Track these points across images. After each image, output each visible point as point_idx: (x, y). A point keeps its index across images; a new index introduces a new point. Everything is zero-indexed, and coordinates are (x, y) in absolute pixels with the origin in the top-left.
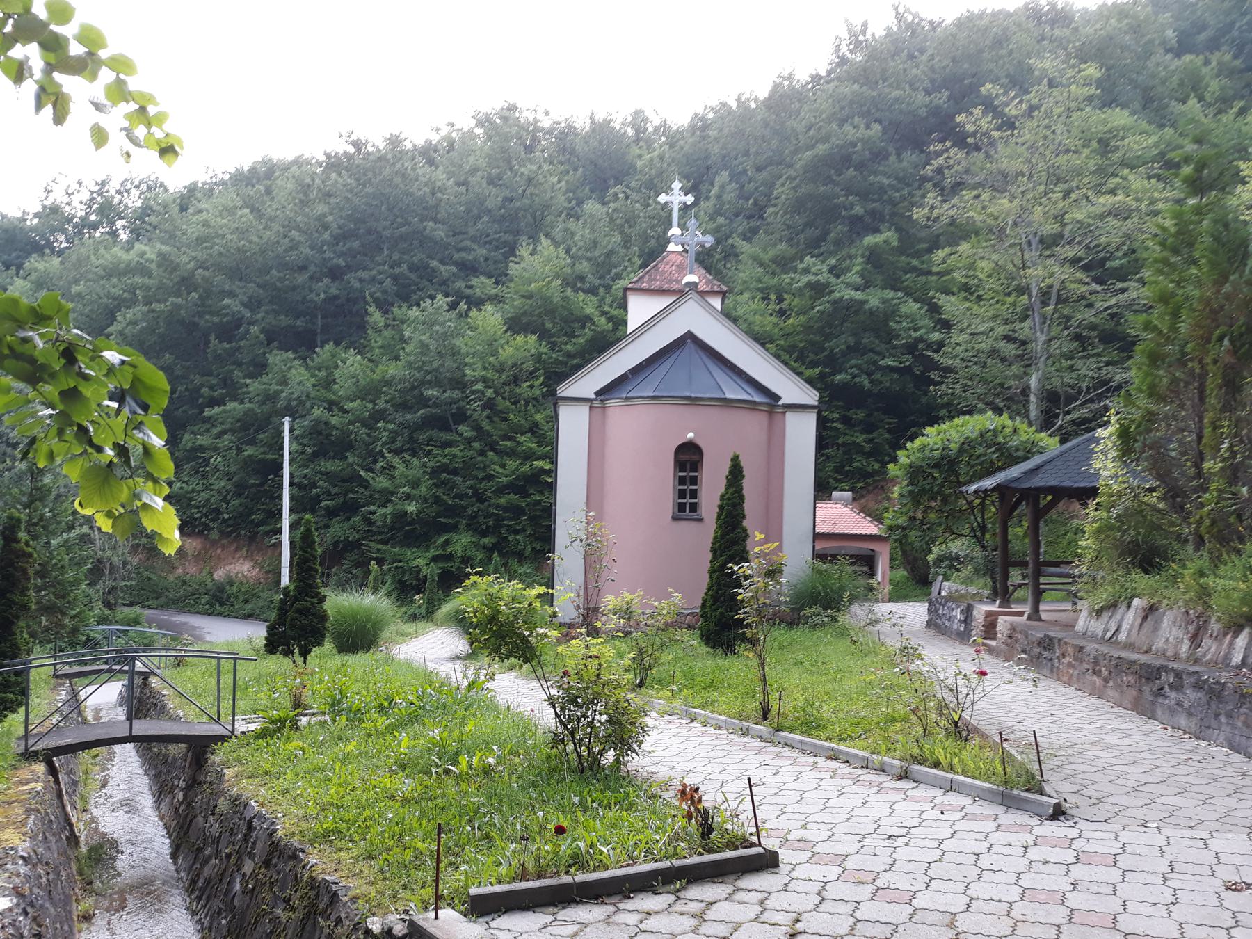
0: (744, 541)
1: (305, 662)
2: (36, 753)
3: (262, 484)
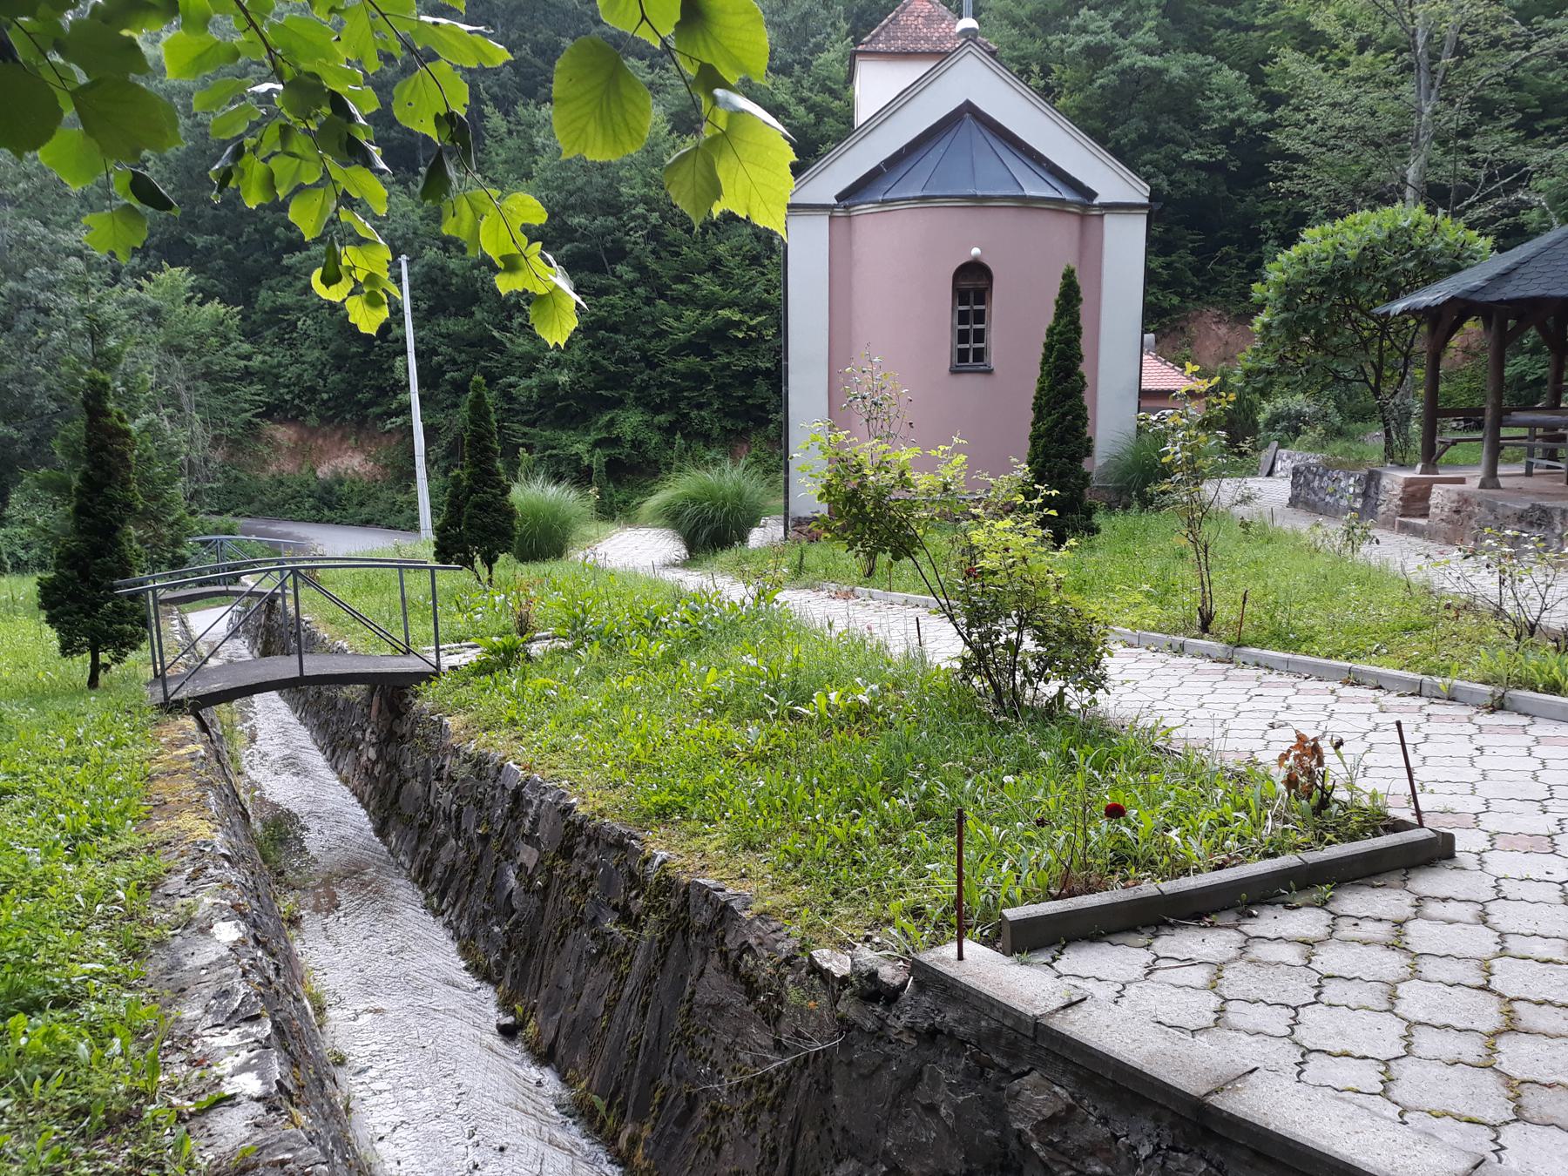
0: (1080, 392)
1: (490, 572)
2: (180, 704)
3: (366, 353)
